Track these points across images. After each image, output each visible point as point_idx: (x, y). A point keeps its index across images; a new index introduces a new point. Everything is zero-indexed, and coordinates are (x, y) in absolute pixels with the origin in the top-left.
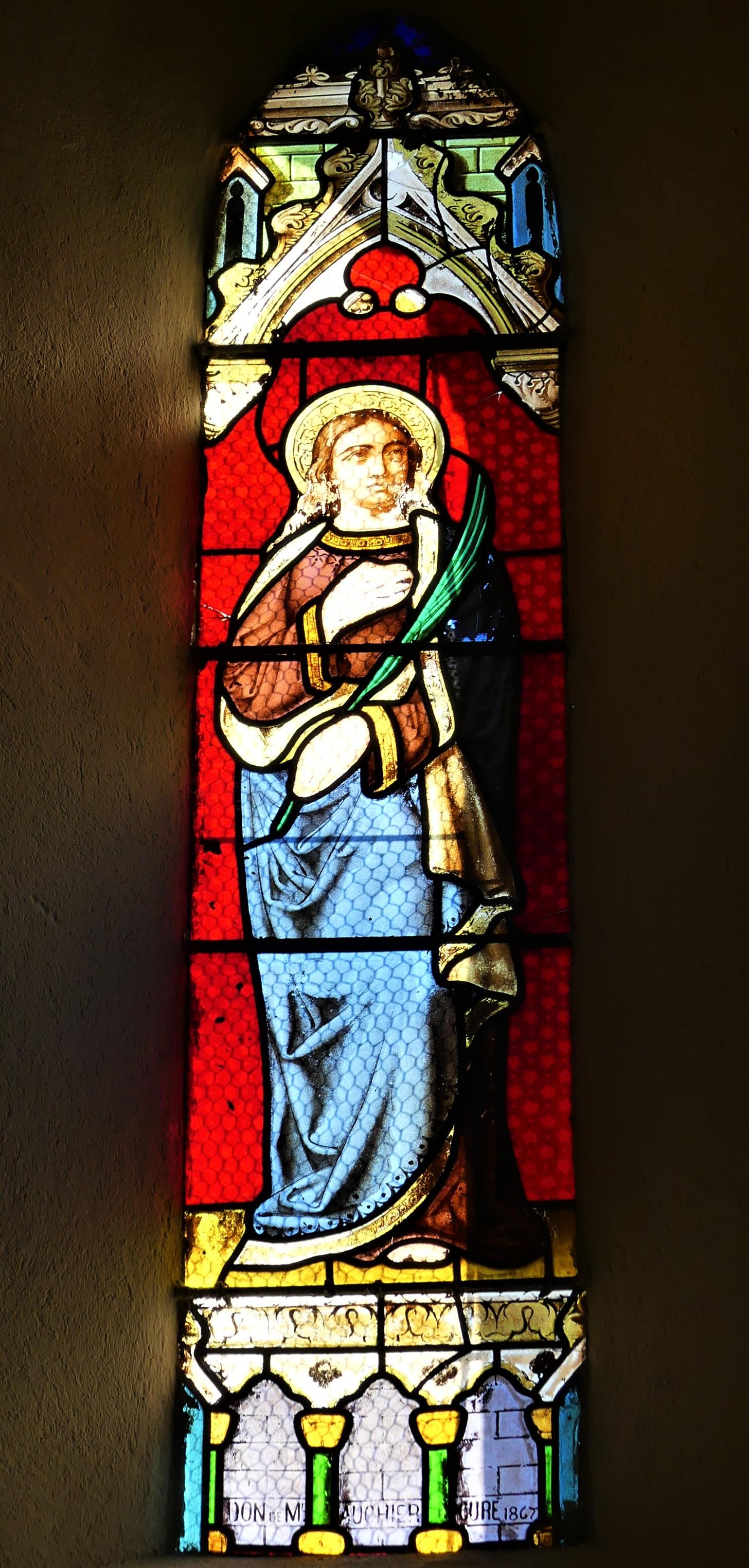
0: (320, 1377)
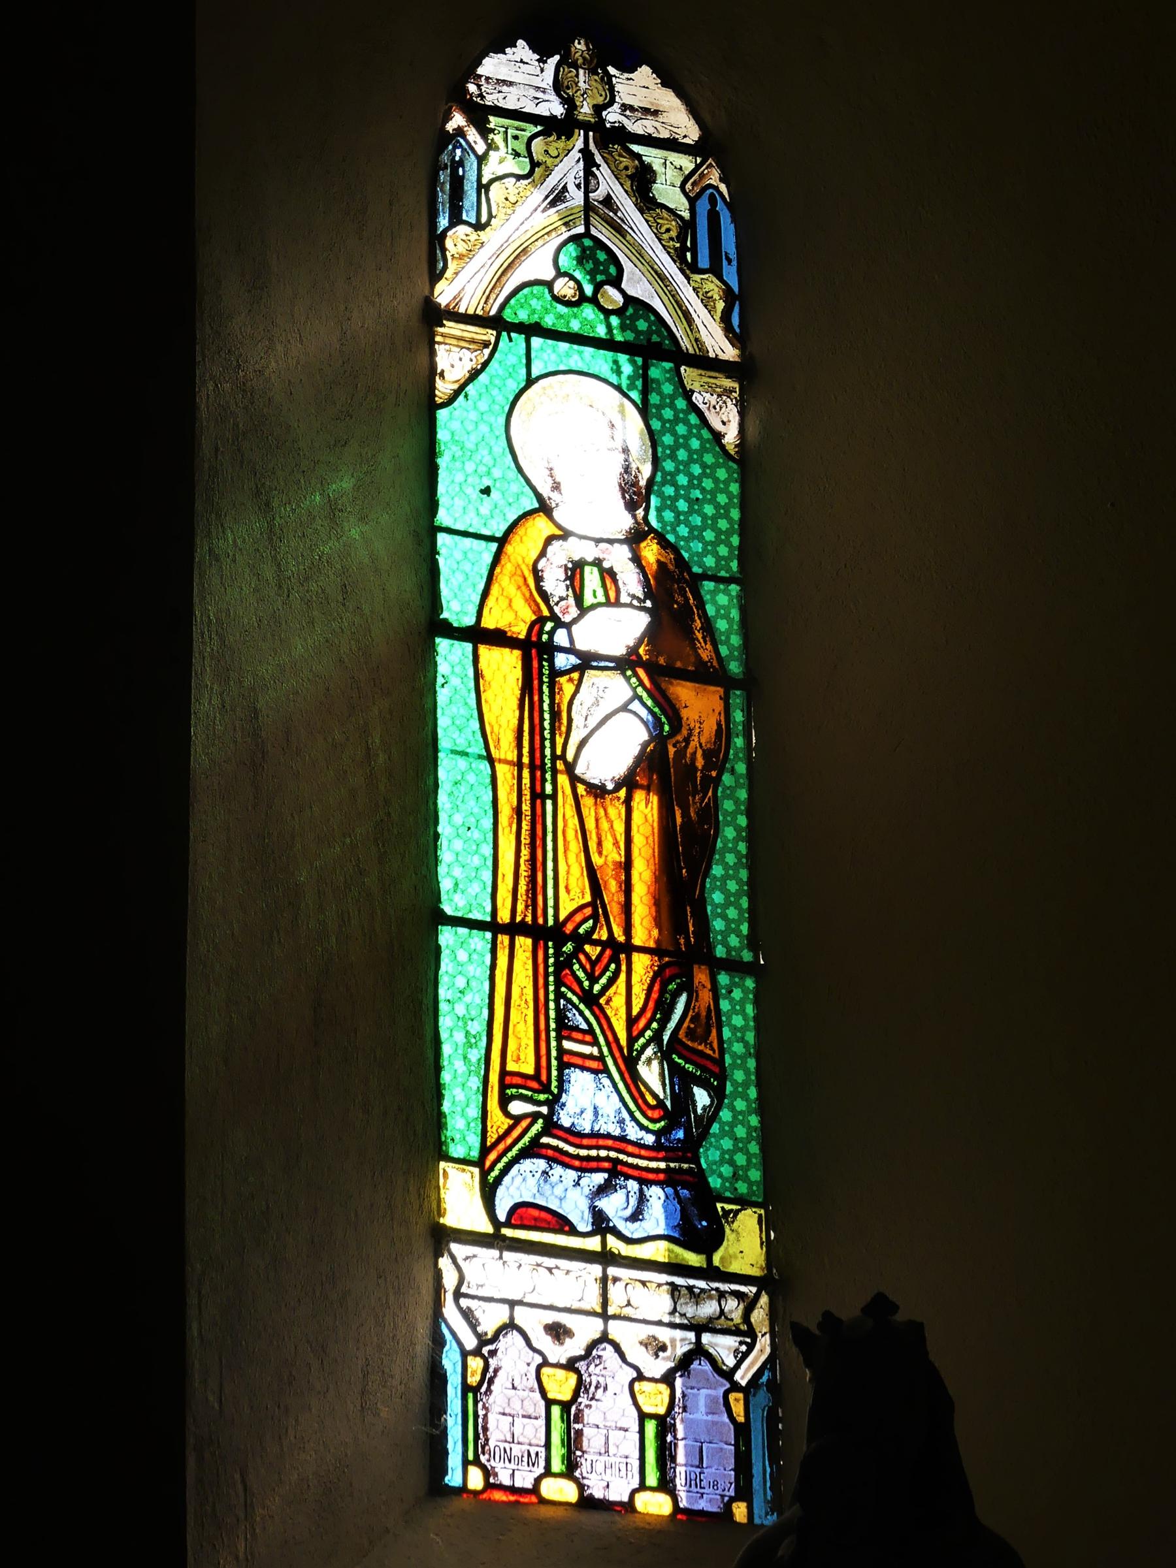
0: (558, 1332)
